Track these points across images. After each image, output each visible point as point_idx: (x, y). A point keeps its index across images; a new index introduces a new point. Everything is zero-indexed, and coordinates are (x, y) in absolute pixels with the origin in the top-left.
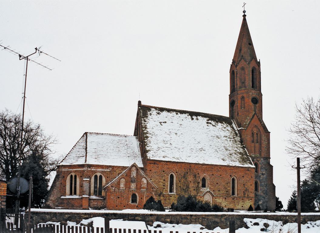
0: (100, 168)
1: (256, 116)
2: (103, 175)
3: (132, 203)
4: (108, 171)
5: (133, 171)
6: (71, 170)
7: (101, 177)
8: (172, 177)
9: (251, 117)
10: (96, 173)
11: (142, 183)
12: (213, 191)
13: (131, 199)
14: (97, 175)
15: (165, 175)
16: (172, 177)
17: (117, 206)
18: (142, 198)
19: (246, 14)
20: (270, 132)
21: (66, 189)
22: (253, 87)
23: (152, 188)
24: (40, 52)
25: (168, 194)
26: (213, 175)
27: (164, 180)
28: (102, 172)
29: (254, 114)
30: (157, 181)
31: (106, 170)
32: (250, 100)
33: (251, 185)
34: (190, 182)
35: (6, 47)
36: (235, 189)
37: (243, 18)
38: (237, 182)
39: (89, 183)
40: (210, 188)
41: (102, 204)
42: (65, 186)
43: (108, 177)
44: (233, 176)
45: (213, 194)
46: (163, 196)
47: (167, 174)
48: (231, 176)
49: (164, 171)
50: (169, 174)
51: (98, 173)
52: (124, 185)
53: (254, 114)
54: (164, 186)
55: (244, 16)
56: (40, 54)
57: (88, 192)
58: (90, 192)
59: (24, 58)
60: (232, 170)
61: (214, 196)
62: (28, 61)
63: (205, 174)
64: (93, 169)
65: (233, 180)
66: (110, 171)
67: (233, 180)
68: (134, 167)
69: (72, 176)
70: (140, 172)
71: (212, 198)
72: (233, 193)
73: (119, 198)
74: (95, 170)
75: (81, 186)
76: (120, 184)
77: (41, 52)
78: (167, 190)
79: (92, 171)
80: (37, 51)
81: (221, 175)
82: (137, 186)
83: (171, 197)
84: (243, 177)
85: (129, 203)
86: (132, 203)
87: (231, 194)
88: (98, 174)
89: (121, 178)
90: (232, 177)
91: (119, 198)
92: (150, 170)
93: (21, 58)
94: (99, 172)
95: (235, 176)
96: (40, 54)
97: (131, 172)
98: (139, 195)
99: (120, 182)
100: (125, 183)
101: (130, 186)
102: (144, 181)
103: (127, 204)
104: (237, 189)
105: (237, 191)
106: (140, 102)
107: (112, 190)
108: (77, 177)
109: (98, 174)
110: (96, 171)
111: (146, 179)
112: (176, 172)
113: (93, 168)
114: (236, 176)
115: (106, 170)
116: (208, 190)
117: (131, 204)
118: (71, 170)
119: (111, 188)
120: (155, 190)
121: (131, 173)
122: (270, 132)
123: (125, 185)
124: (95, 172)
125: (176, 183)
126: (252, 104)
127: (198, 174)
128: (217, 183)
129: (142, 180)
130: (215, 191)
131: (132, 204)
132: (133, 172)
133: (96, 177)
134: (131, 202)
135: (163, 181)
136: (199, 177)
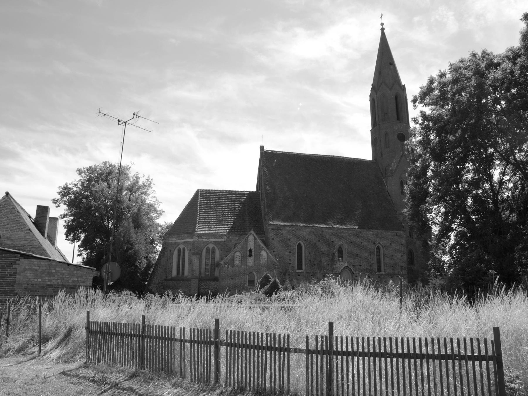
1: (404, 157)
2: (217, 247)
4: (223, 242)
5: (250, 241)
6: (179, 241)
8: (300, 246)
9: (399, 160)
11: (261, 258)
12: (353, 265)
14: (209, 247)
15: (292, 245)
16: (300, 246)
19: (384, 26)
21: (172, 268)
22: (398, 118)
23: (274, 264)
24: (137, 117)
25: (296, 272)
26: (351, 242)
27: (290, 252)
28: (216, 243)
29: (401, 154)
30: (281, 253)
32: (396, 137)
33: (402, 256)
34: (323, 254)
35: (105, 114)
36: (381, 262)
37: (381, 32)
38: (383, 252)
39: (200, 259)
40: (349, 262)
41: (214, 288)
44: (377, 244)
45: (353, 270)
46: (289, 275)
47: (294, 244)
48: (374, 243)
49: (289, 240)
50: (296, 243)
51: (211, 244)
52: (239, 261)
53: (402, 155)
54: (290, 260)
55: (383, 30)
56: (138, 118)
57: (198, 271)
58: (201, 272)
59: (123, 123)
60: (376, 235)
61: (353, 273)
62: (126, 125)
63: (341, 243)
64: (204, 240)
65: (378, 248)
66: (225, 242)
67: (378, 248)
68: (238, 252)
69: (179, 250)
70: (258, 242)
71: (352, 275)
72: (379, 269)
73: (232, 279)
74: (206, 240)
75: (190, 263)
76: (234, 260)
77: (139, 117)
78: (294, 266)
80: (135, 116)
81: (361, 243)
82: (254, 262)
83: (299, 276)
84: (391, 244)
85: (246, 285)
86: (248, 286)
87: (376, 270)
88: (211, 246)
89: (235, 252)
90: (376, 245)
91: (232, 279)
92: (273, 239)
93: (120, 123)
95: (379, 243)
96: (138, 118)
97: (247, 243)
98: (257, 274)
99: (234, 257)
100: (240, 257)
101: (246, 263)
102: (264, 253)
104: (384, 262)
105: (384, 265)
106: (262, 148)
107: (225, 269)
109: (211, 246)
110: (209, 241)
111: (266, 251)
112: (305, 240)
113: (205, 237)
114: (381, 243)
115: (220, 240)
116: (346, 265)
117: (247, 287)
118: (179, 241)
119: (224, 265)
120: (277, 267)
121: (248, 244)
123: (241, 261)
124: (208, 243)
125: (305, 256)
126: (398, 141)
127: (333, 242)
128: (357, 255)
129: (261, 253)
130: (355, 266)
132: (250, 243)
133: (208, 250)
134: (247, 284)
135: (289, 253)
136: (334, 246)
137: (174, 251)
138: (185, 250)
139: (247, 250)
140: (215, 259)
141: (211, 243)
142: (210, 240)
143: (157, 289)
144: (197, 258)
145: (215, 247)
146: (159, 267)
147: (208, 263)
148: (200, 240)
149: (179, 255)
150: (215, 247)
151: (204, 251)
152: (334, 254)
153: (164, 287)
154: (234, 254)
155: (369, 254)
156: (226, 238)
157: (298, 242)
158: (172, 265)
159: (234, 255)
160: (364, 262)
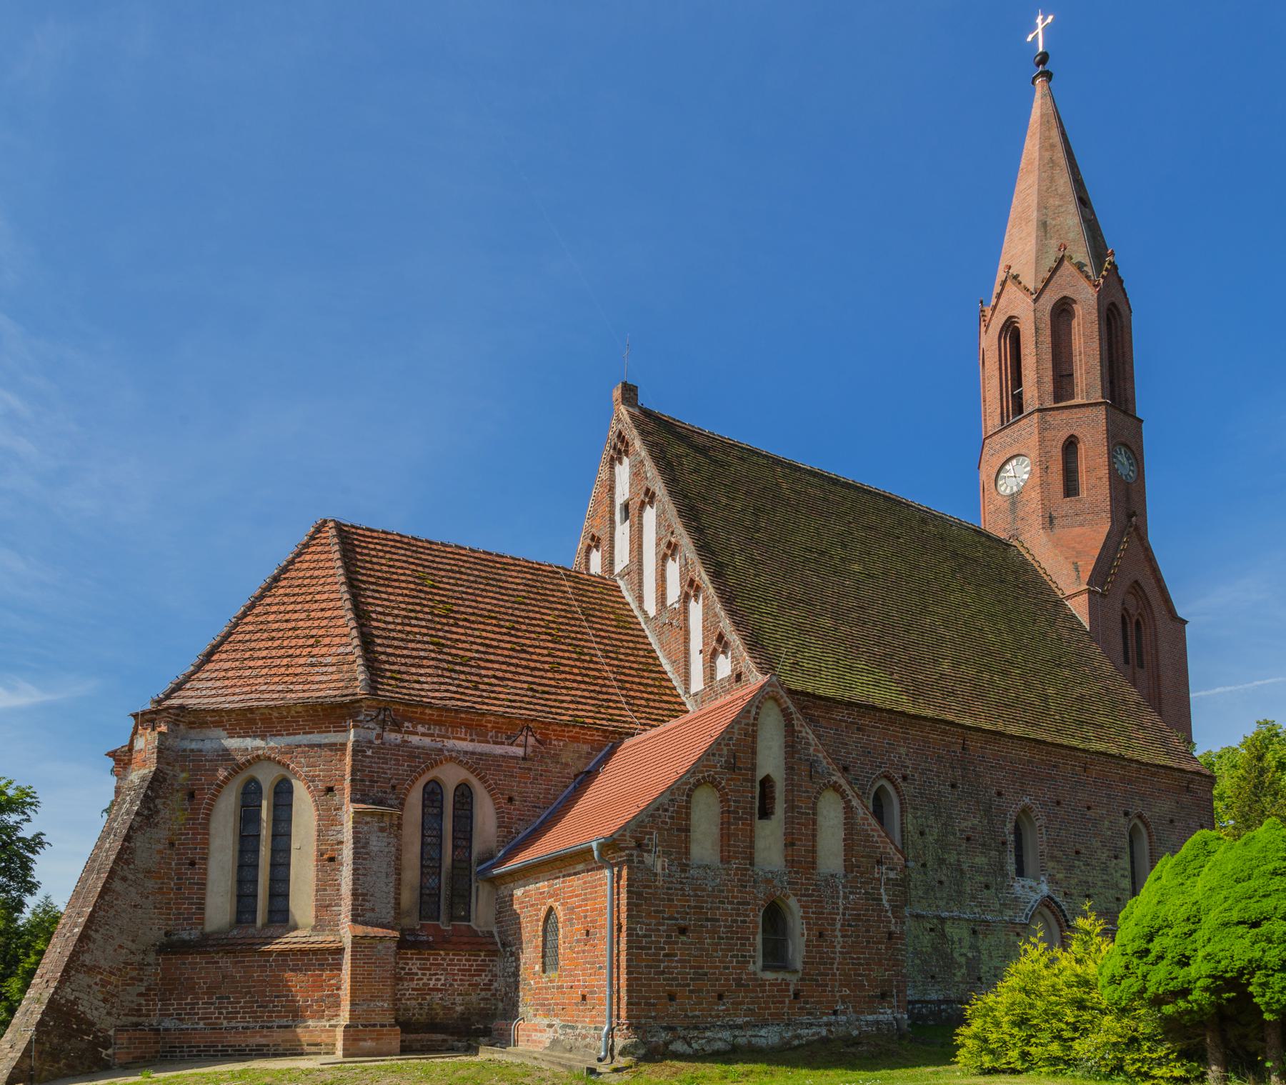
0: (462, 732)
3: (765, 968)
4: (516, 758)
7: (464, 794)
10: (436, 764)
12: (1066, 894)
13: (759, 938)
17: (672, 997)
18: (821, 935)
20: (1187, 622)
21: (203, 885)
26: (1058, 803)
28: (477, 764)
31: (499, 750)
40: (1052, 880)
42: (196, 862)
43: (511, 800)
63: (1027, 800)
64: (415, 740)
66: (524, 759)
73: (683, 931)
75: (332, 859)
79: (413, 754)
85: (751, 967)
86: (765, 968)
88: (451, 776)
94: (456, 758)
103: (738, 982)
108: (300, 789)
109: (451, 776)
111: (843, 795)
113: (420, 729)
114: (1146, 814)
115: (499, 750)
116: (1045, 889)
117: (761, 975)
122: (1187, 622)
123: (726, 836)
124: (435, 758)
127: (999, 794)
130: (1071, 895)
131: (769, 976)
133: (433, 793)
134: (760, 962)
137: (215, 797)
138: (290, 791)
139: (753, 781)
140: (470, 840)
141: (451, 759)
142: (450, 743)
143: (105, 1000)
144: (382, 830)
145: (475, 782)
146: (124, 879)
147: (432, 859)
148: (393, 737)
149: (248, 816)
150: (475, 782)
151: (415, 797)
152: (1004, 843)
153: (148, 989)
154: (689, 796)
155: (1112, 854)
156: (531, 740)
157: (877, 785)
158: (205, 872)
159: (688, 802)
160: (1100, 884)
